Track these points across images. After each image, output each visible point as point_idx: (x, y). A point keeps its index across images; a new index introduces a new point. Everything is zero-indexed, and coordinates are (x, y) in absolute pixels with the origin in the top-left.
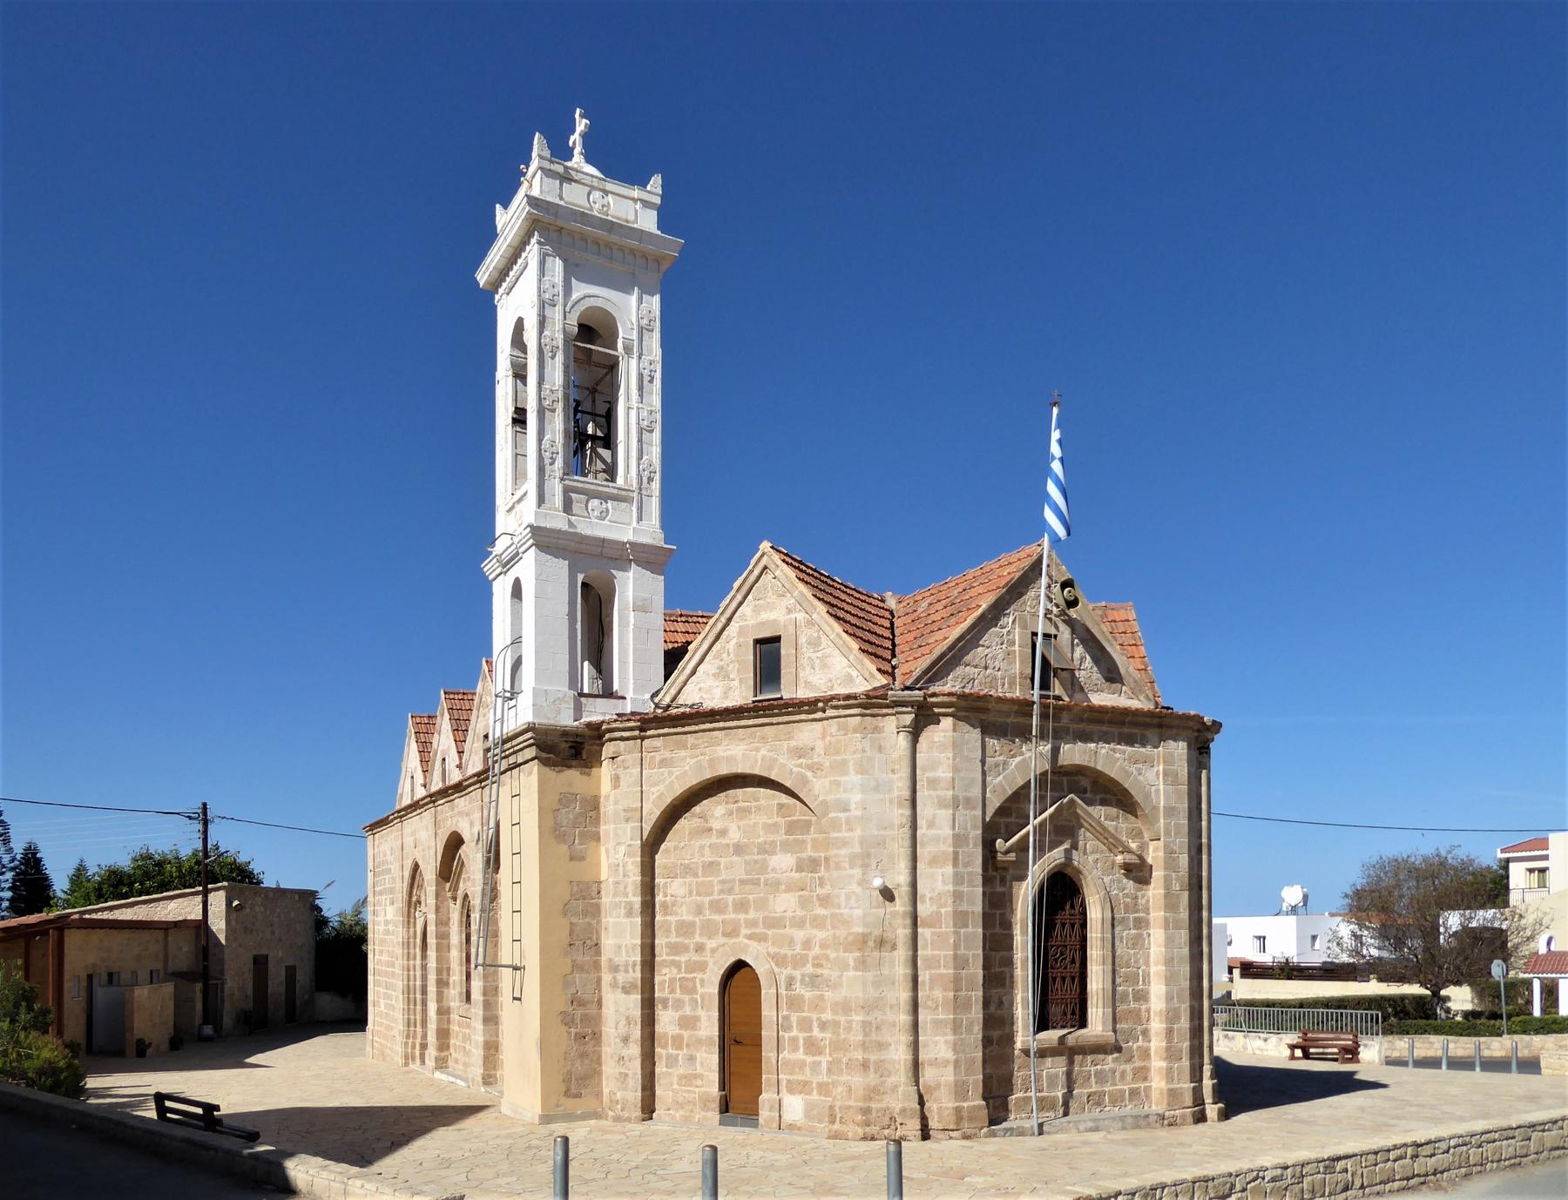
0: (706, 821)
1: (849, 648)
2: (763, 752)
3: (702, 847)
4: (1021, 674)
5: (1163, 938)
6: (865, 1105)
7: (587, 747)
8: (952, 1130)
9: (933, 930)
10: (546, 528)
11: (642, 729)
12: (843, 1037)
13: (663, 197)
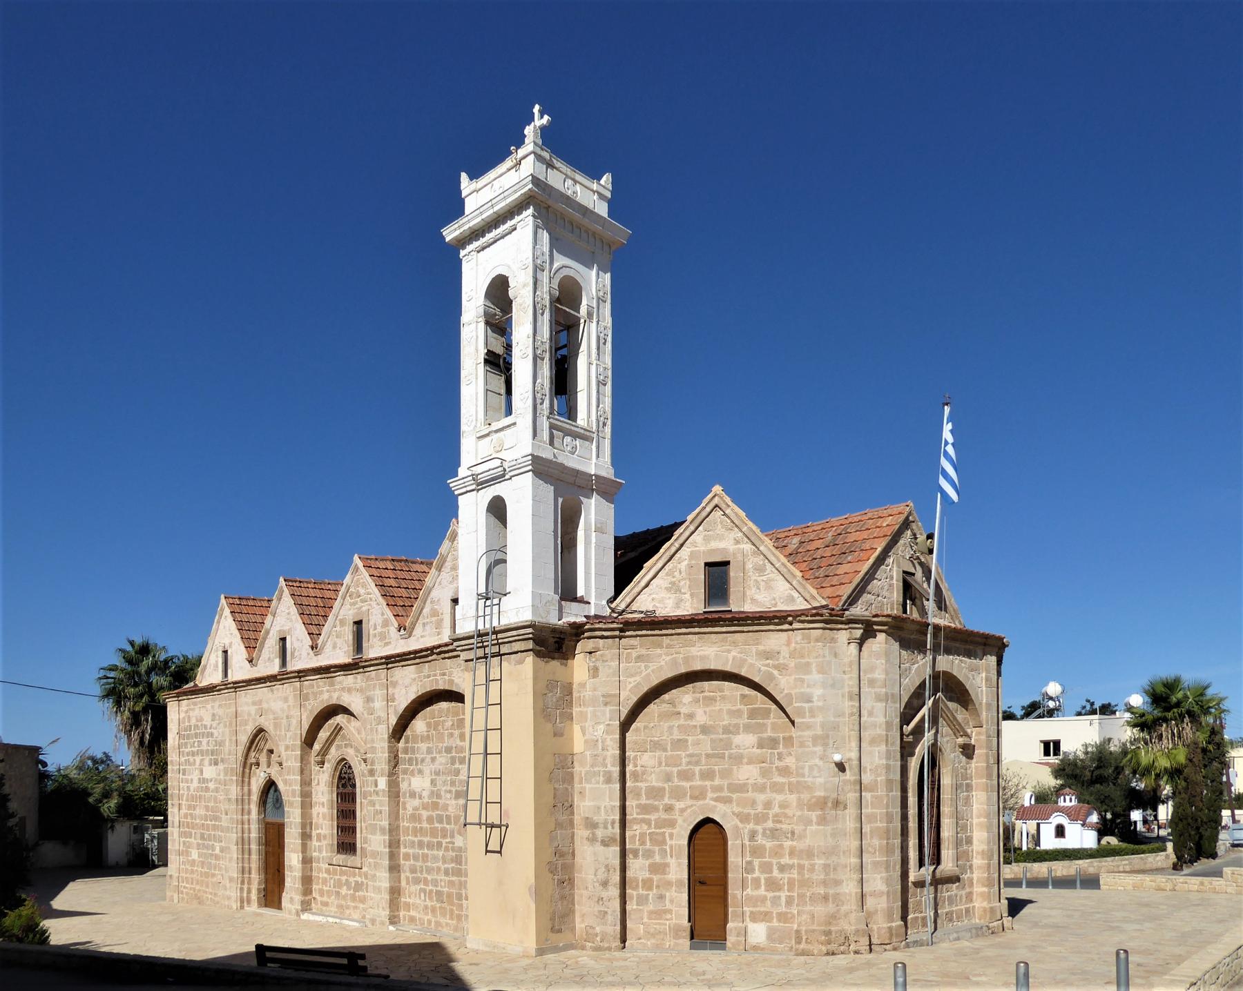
0: (675, 706)
1: (793, 574)
2: (734, 653)
3: (671, 728)
4: (897, 601)
5: (985, 798)
6: (827, 929)
7: (566, 642)
8: (886, 944)
9: (873, 794)
10: (542, 458)
11: (621, 630)
12: (807, 876)
13: (612, 193)
